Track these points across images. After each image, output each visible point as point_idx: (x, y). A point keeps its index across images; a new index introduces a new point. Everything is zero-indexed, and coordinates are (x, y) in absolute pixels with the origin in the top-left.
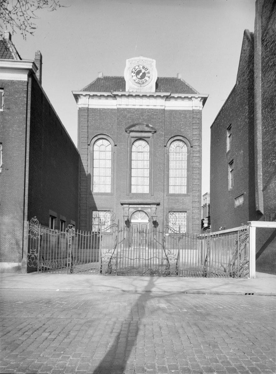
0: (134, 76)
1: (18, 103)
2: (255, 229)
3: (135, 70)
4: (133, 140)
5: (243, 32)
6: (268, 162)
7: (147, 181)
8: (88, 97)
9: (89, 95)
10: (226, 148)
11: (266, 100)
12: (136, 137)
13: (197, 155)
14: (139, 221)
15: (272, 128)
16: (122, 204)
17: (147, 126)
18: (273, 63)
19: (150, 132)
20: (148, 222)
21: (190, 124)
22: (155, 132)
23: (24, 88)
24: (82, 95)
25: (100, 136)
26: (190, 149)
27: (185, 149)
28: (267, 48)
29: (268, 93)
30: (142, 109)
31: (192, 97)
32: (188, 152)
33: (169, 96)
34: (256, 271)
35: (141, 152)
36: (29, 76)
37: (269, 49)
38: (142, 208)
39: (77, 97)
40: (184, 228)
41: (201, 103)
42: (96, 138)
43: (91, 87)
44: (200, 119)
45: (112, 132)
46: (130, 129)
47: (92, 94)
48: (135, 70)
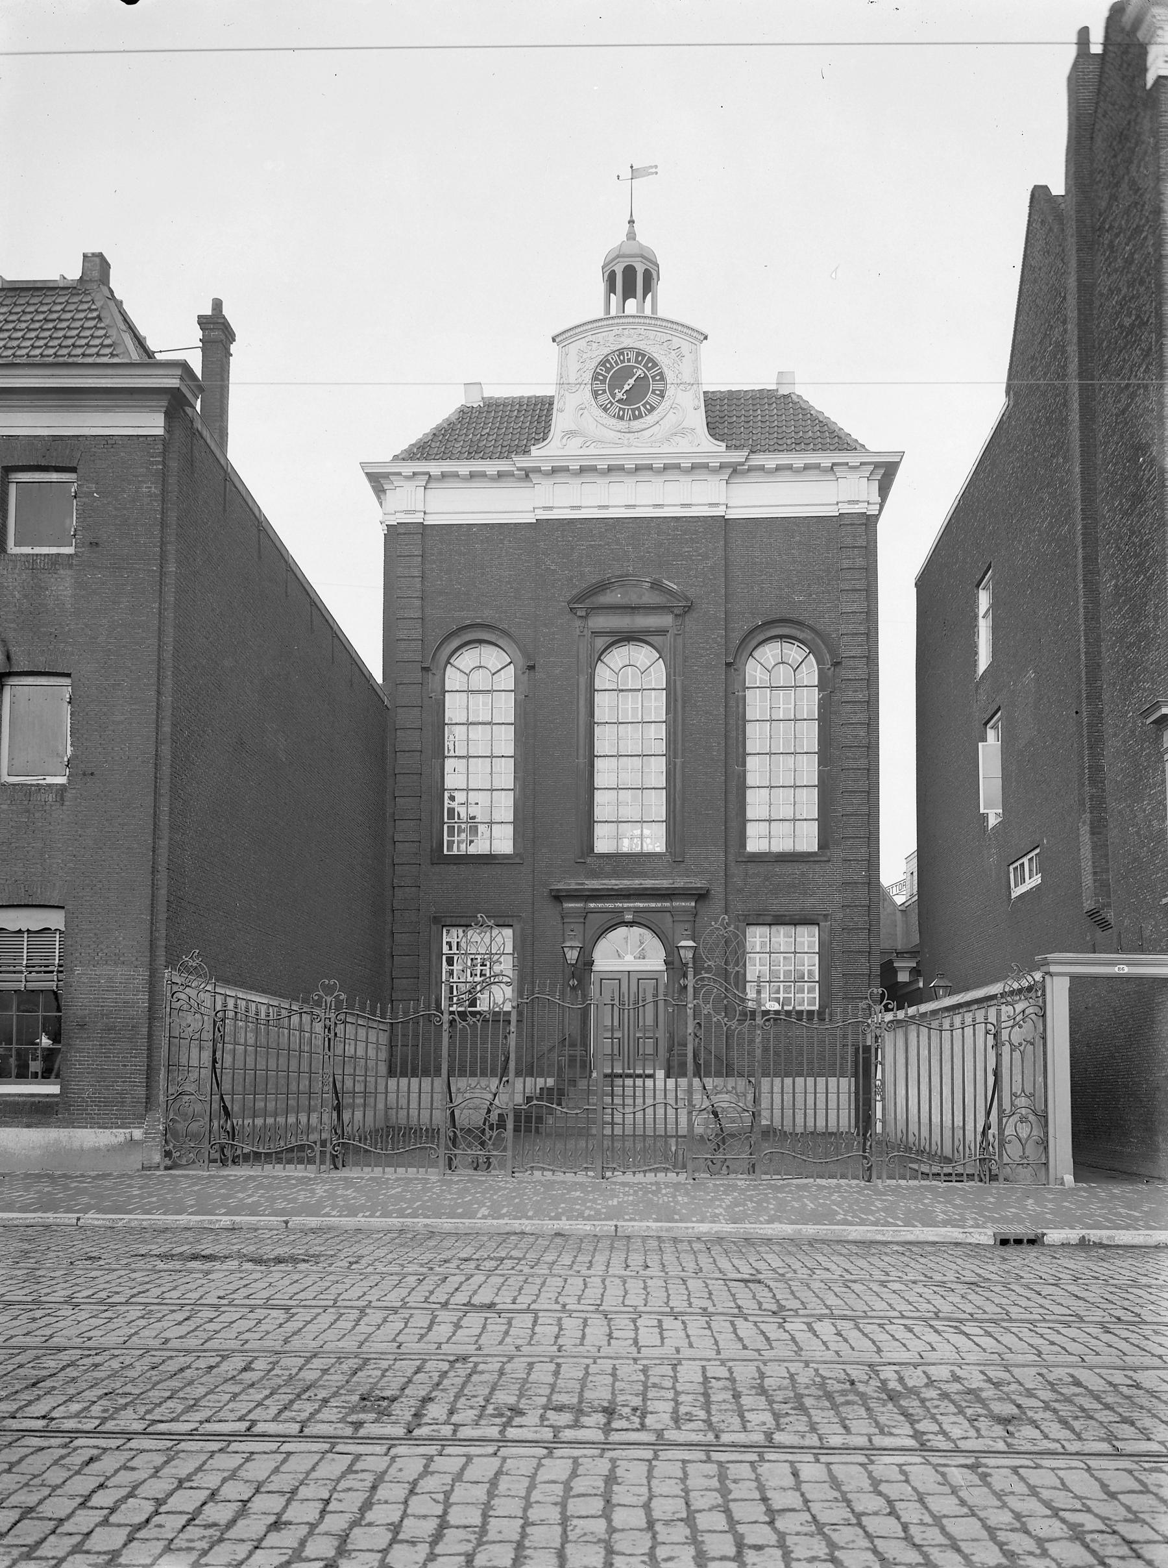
1: (131, 521)
2: (1065, 982)
3: (608, 371)
4: (600, 642)
5: (1028, 200)
6: (1127, 712)
7: (657, 805)
8: (424, 483)
9: (428, 473)
10: (975, 664)
11: (1115, 465)
12: (611, 633)
13: (860, 696)
14: (630, 962)
15: (1137, 574)
16: (558, 897)
17: (656, 586)
18: (1138, 317)
20: (664, 968)
22: (688, 609)
23: (152, 463)
24: (399, 474)
25: (473, 633)
26: (830, 673)
27: (810, 673)
28: (1116, 259)
29: (1122, 437)
31: (834, 464)
32: (821, 686)
33: (742, 464)
34: (1149, 1179)
35: (631, 690)
36: (169, 416)
37: (1120, 263)
39: (378, 481)
40: (785, 992)
41: (875, 486)
42: (456, 643)
43: (421, 451)
44: (869, 551)
46: (588, 603)
47: (435, 468)
48: (608, 371)
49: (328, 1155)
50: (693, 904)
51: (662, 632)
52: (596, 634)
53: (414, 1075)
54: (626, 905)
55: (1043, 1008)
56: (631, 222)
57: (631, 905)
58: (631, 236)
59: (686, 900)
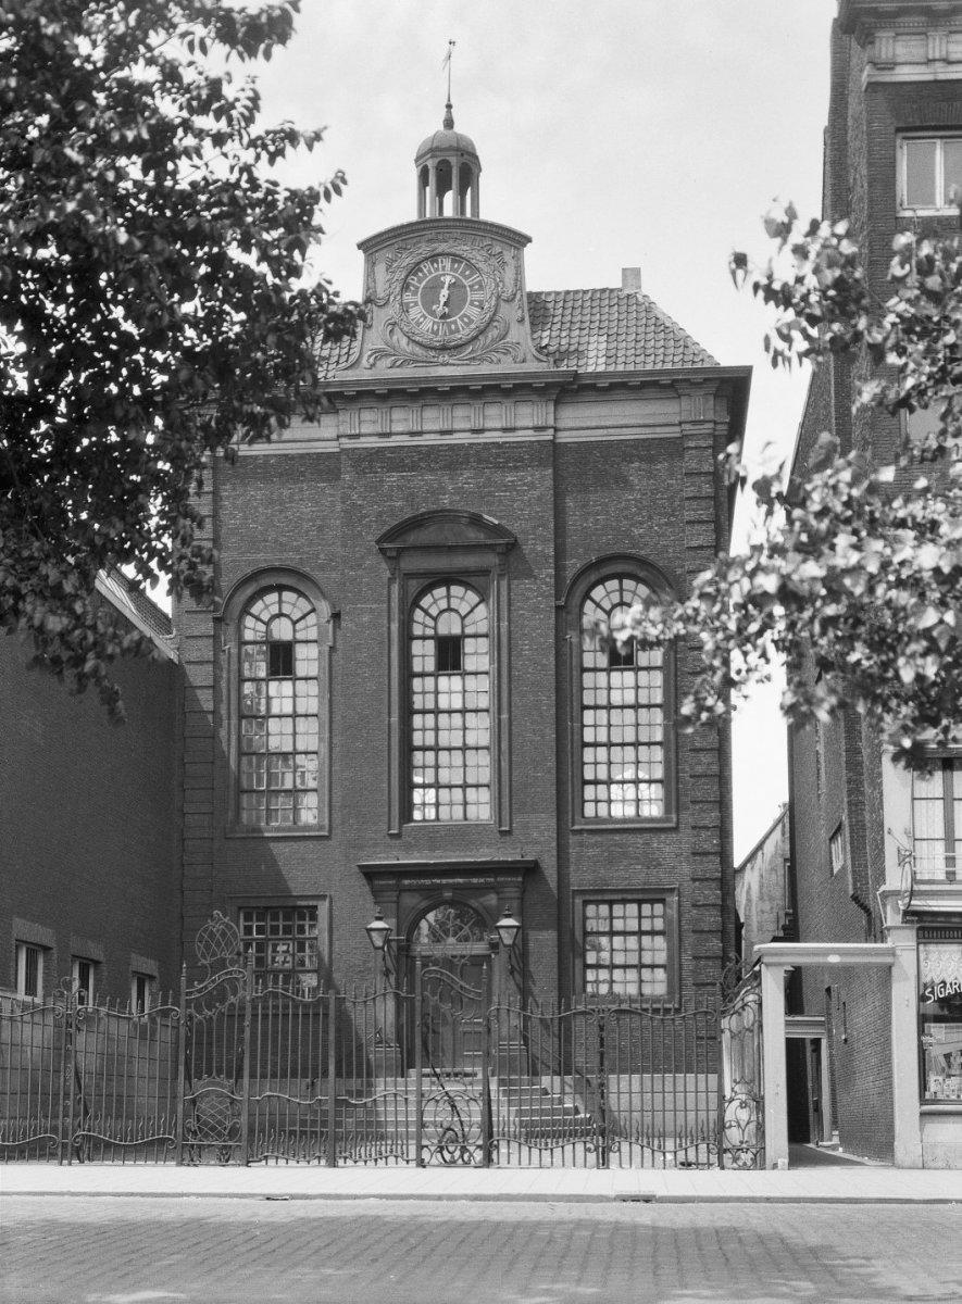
0: (416, 304)
4: (414, 586)
19: (491, 547)
21: (671, 499)
30: (451, 447)
38: (455, 887)
42: (250, 590)
45: (322, 556)
49: (69, 1148)
50: (520, 879)
51: (485, 572)
52: (409, 576)
53: (689, 1070)
54: (444, 881)
55: (760, 998)
56: (449, 107)
57: (451, 881)
58: (449, 123)
59: (389, 879)
